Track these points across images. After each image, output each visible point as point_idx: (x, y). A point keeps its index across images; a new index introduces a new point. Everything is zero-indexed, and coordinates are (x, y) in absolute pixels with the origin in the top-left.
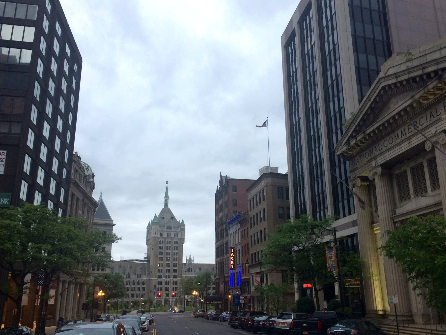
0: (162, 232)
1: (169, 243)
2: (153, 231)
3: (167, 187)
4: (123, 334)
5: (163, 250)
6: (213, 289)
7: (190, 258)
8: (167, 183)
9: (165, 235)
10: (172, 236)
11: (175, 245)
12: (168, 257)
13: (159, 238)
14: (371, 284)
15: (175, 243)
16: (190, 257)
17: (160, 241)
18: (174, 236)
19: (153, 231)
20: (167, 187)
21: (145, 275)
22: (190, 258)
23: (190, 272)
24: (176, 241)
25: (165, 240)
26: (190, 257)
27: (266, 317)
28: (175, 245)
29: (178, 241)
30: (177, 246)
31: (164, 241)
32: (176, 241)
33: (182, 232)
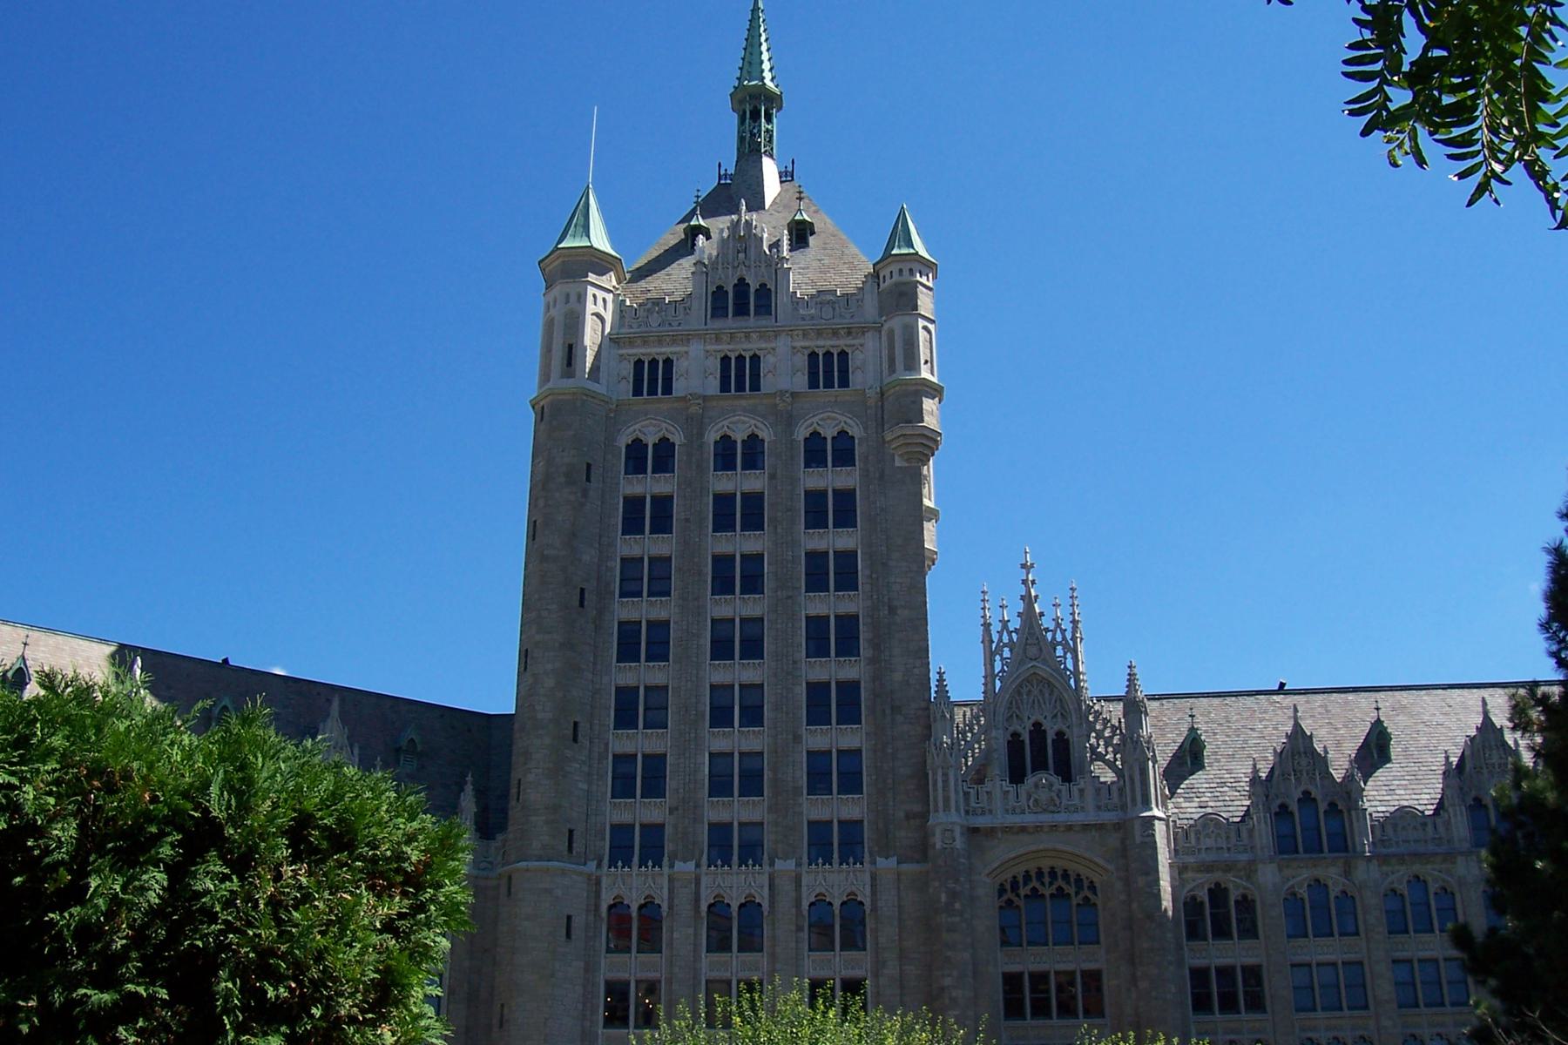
7: (1029, 617)
16: (1028, 600)
22: (1029, 617)
26: (1028, 600)
28: (830, 479)
31: (677, 438)
33: (896, 323)
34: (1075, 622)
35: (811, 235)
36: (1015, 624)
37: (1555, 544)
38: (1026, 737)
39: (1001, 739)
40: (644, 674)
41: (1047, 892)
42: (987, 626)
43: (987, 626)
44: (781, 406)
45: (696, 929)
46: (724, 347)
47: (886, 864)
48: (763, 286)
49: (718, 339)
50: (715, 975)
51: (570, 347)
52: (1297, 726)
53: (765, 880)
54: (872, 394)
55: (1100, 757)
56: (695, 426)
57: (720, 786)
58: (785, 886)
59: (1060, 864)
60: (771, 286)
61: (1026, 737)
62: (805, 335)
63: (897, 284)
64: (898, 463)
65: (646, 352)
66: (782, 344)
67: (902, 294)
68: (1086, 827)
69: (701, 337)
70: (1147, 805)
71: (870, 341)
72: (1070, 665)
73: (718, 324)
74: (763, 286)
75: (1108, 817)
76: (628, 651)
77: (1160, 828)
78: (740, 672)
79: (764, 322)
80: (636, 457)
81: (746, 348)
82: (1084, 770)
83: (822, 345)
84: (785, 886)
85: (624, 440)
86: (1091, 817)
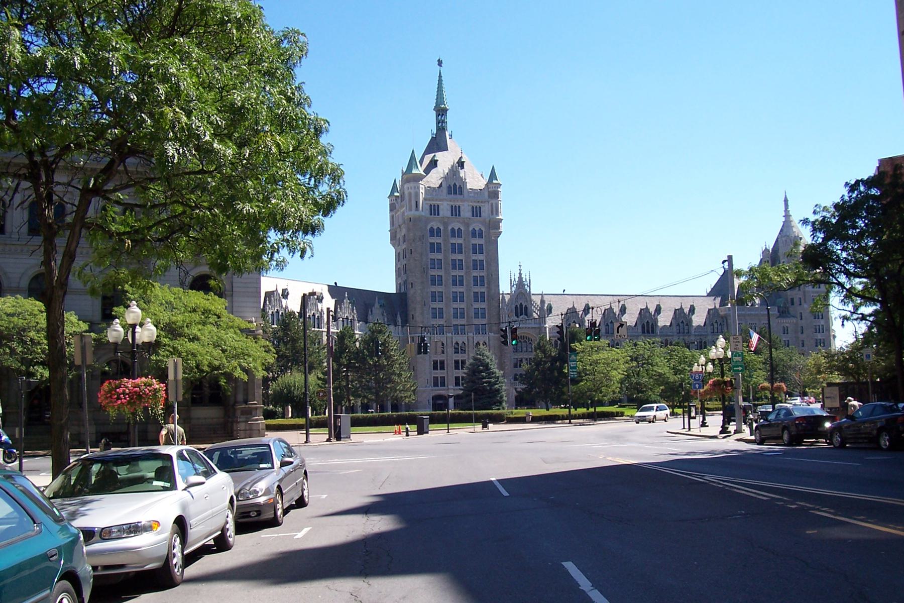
0: (478, 205)
1: (456, 233)
2: (410, 201)
3: (440, 76)
4: (903, 435)
5: (442, 254)
6: (457, 384)
7: (520, 278)
8: (440, 63)
9: (445, 211)
10: (466, 212)
11: (477, 241)
12: (457, 273)
13: (427, 221)
14: (610, 420)
15: (474, 233)
16: (520, 274)
17: (453, 228)
18: (469, 214)
19: (410, 201)
20: (440, 76)
21: (396, 325)
22: (520, 278)
23: (523, 316)
24: (456, 229)
25: (446, 225)
26: (520, 274)
27: (266, 517)
28: (477, 241)
29: (483, 229)
30: (481, 241)
31: (442, 228)
32: (456, 229)
33: (494, 201)
34: (530, 280)
35: (759, 338)
36: (517, 280)
37: (444, 173)
38: (519, 306)
39: (514, 306)
40: (437, 289)
41: (522, 341)
42: (511, 280)
43: (511, 280)
44: (466, 221)
45: (822, 283)
46: (452, 203)
47: (492, 334)
48: (460, 186)
49: (451, 201)
50: (464, 354)
51: (417, 202)
52: (647, 306)
53: (466, 338)
54: (487, 220)
55: (535, 312)
56: (446, 225)
57: (456, 316)
58: (471, 339)
59: (525, 335)
60: (462, 186)
61: (519, 306)
62: (471, 202)
63: (495, 191)
64: (493, 238)
65: (433, 203)
66: (466, 204)
67: (496, 194)
68: (532, 328)
69: (446, 200)
70: (545, 324)
71: (486, 204)
72: (528, 290)
73: (450, 196)
74: (460, 186)
75: (536, 326)
76: (433, 283)
77: (547, 329)
78: (459, 289)
79: (461, 197)
80: (432, 232)
81: (457, 204)
82: (532, 315)
83: (475, 204)
84: (449, 341)
85: (429, 228)
86: (534, 326)
